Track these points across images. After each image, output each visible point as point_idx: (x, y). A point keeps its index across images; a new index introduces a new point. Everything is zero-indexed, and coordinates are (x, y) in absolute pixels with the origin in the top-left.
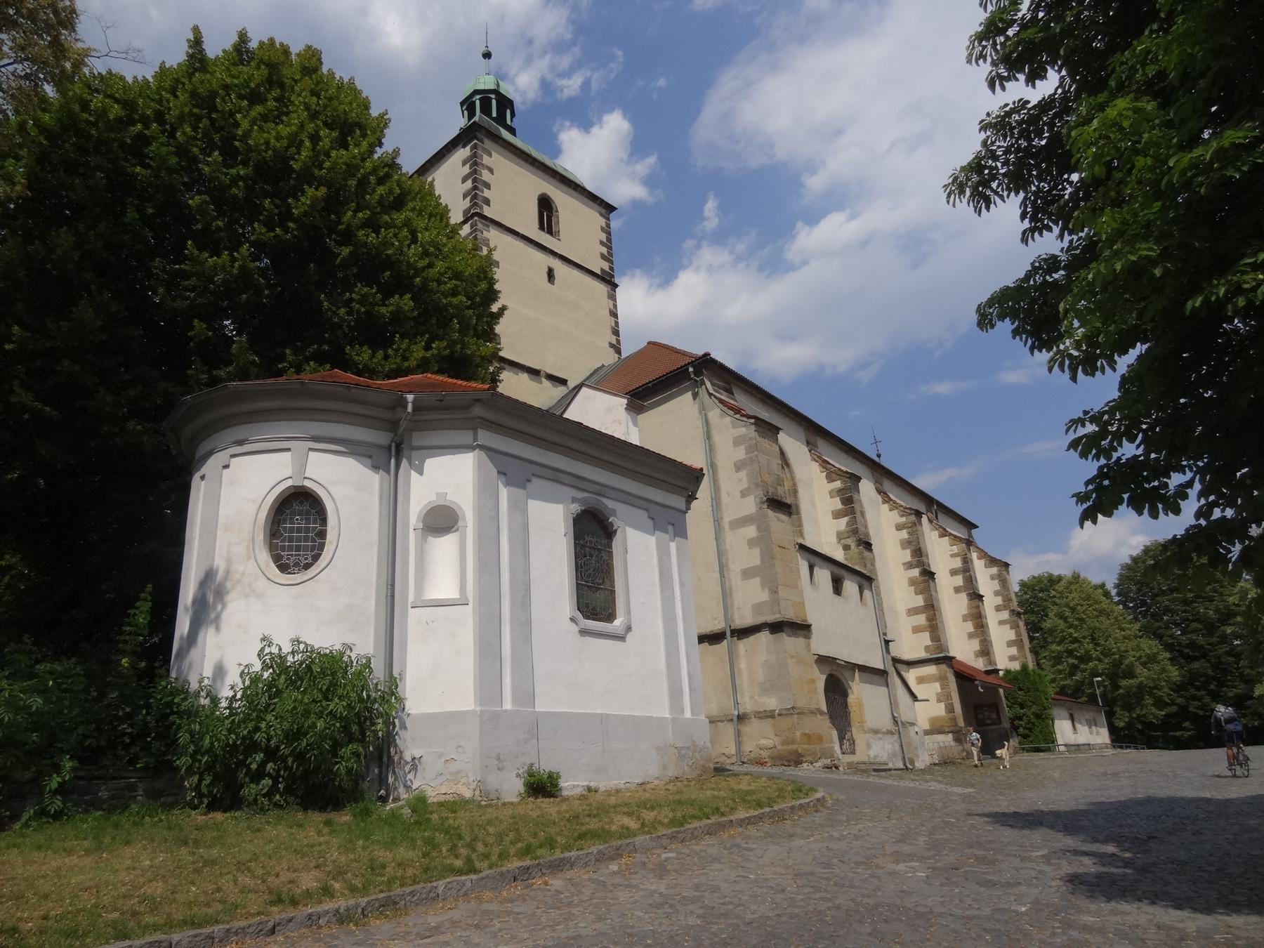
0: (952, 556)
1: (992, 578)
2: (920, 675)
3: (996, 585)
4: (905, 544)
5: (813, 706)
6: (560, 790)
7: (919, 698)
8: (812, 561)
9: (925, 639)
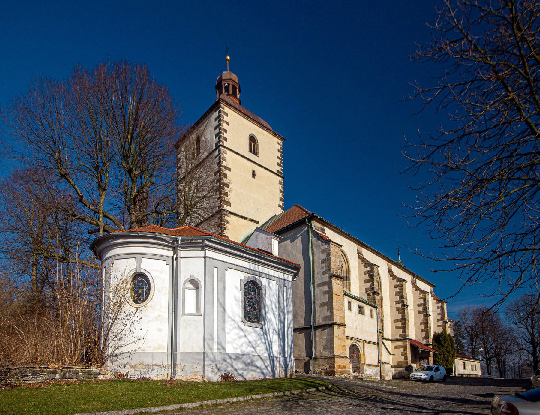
0: (420, 298)
1: (438, 308)
2: (396, 345)
8: (350, 301)
9: (400, 331)
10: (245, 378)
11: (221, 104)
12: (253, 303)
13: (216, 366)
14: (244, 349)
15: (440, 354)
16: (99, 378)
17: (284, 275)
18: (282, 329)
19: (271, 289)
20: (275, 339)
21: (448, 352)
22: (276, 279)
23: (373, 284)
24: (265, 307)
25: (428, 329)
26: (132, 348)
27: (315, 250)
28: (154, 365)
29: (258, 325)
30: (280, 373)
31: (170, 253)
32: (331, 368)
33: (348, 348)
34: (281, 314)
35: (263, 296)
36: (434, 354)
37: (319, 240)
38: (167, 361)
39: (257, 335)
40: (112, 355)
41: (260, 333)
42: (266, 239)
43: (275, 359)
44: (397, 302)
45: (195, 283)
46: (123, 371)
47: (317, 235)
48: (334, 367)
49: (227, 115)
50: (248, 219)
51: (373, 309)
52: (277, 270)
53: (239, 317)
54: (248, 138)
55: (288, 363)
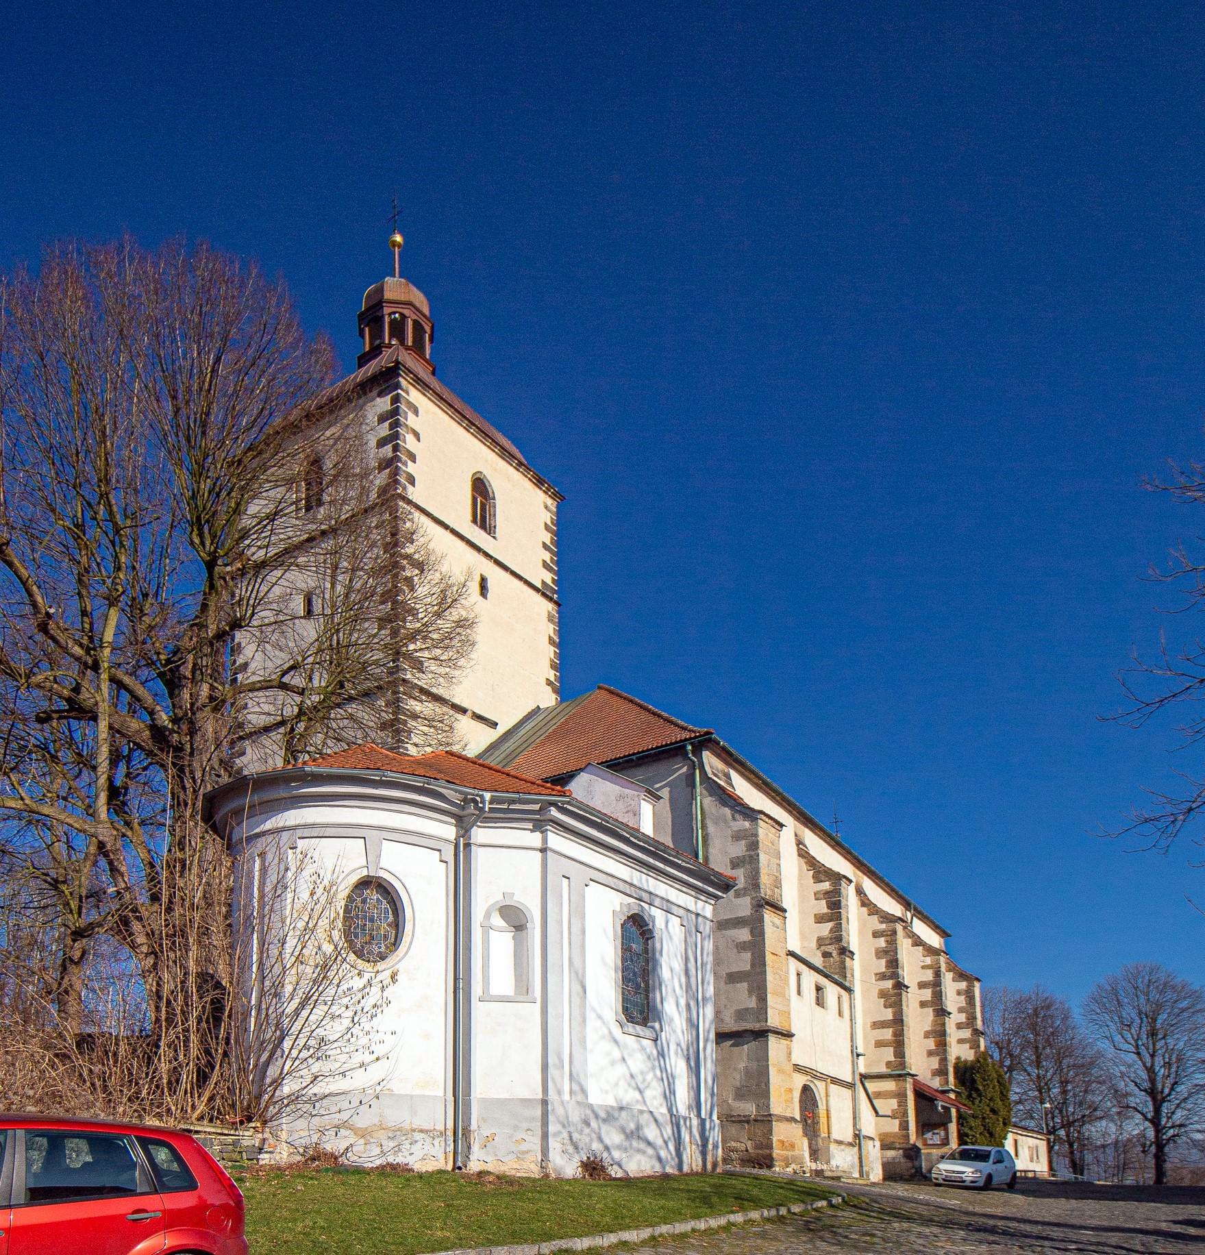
0: (923, 967)
1: (959, 993)
3: (962, 1001)
4: (880, 953)
5: (788, 1115)
6: (1165, 1161)
7: (880, 1114)
9: (889, 1054)
11: (401, 379)
13: (571, 1138)
14: (621, 1093)
16: (261, 1163)
17: (696, 903)
18: (695, 1046)
19: (671, 938)
20: (679, 1067)
21: (993, 1111)
22: (681, 912)
23: (838, 927)
24: (660, 985)
25: (945, 1050)
26: (358, 1080)
27: (711, 829)
28: (414, 1131)
29: (648, 1033)
30: (692, 1160)
31: (449, 831)
32: (761, 1149)
33: (797, 1095)
34: (692, 1004)
35: (657, 955)
36: (960, 1117)
37: (725, 804)
38: (438, 1116)
39: (645, 1057)
40: (295, 1098)
41: (652, 1053)
42: (621, 797)
43: (682, 1122)
45: (515, 918)
46: (333, 1145)
48: (770, 1147)
50: (469, 713)
51: (843, 992)
52: (684, 889)
53: (611, 1009)
54: (470, 483)
55: (707, 1133)
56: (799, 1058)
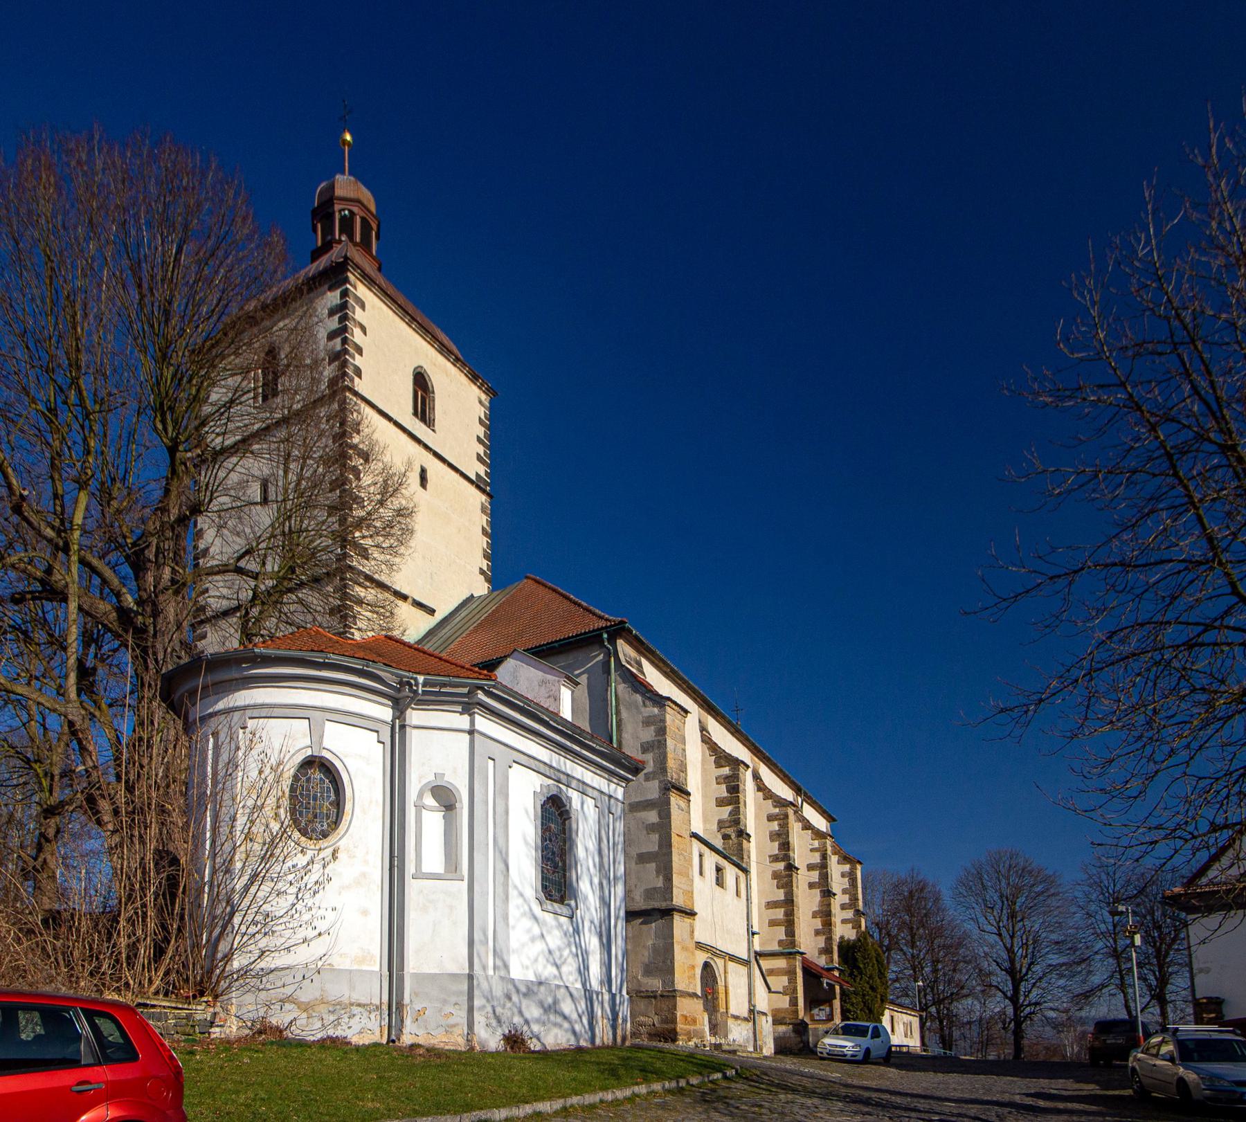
0: (812, 850)
1: (843, 875)
5: (691, 991)
9: (780, 933)
10: (543, 1044)
11: (349, 274)
12: (553, 853)
15: (855, 993)
16: (213, 1036)
20: (592, 943)
21: (872, 988)
22: (596, 794)
25: (831, 930)
26: (302, 956)
27: (624, 714)
28: (352, 1004)
30: (604, 1034)
31: (385, 712)
33: (698, 971)
34: (605, 882)
36: (844, 993)
37: (636, 691)
38: (375, 991)
40: (244, 972)
42: (543, 682)
44: (775, 859)
45: (445, 797)
46: (278, 1018)
47: (632, 679)
48: (674, 1021)
49: (363, 307)
50: (410, 600)
51: (740, 873)
52: (598, 772)
56: (701, 936)
